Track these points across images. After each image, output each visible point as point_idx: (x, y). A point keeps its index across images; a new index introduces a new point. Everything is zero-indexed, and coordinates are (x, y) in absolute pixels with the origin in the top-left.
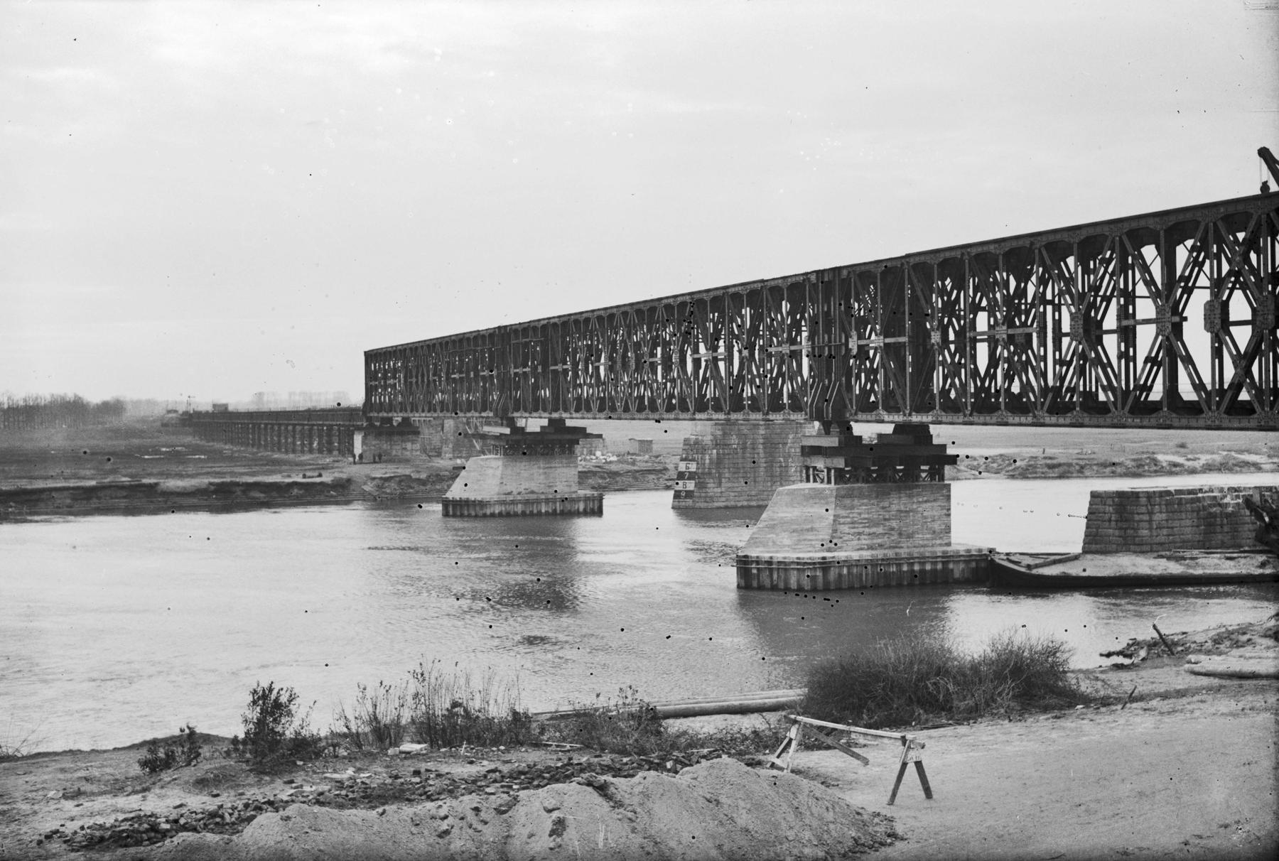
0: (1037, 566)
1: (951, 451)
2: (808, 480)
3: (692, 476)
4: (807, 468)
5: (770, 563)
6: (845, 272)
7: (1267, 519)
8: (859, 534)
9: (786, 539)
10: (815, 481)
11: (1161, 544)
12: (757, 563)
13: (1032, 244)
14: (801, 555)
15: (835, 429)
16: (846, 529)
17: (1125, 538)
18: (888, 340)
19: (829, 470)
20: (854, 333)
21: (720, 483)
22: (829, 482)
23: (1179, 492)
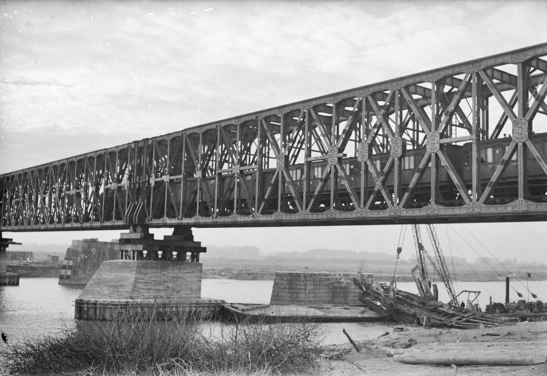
0: (248, 310)
1: (203, 245)
2: (122, 258)
3: (70, 268)
4: (122, 251)
5: (95, 304)
6: (150, 142)
7: (364, 289)
8: (149, 289)
9: (106, 291)
10: (126, 258)
11: (310, 302)
12: (87, 304)
13: (257, 117)
14: (114, 300)
15: (139, 229)
16: (142, 286)
17: (292, 298)
18: (172, 178)
19: (134, 252)
20: (153, 175)
21: (85, 272)
22: (134, 259)
23: (319, 275)
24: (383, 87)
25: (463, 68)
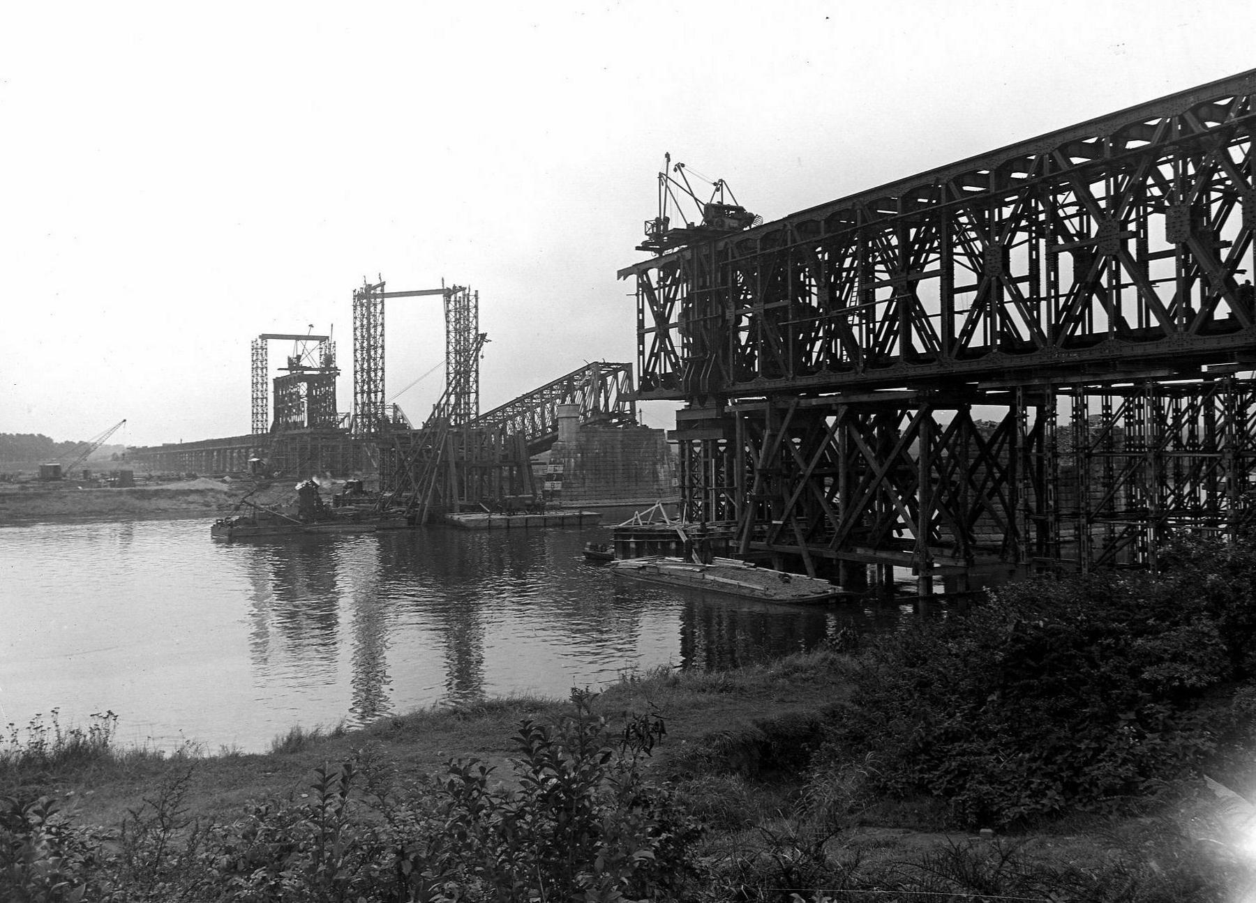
3: (559, 477)
18: (768, 306)
24: (1022, 151)
25: (1155, 110)
